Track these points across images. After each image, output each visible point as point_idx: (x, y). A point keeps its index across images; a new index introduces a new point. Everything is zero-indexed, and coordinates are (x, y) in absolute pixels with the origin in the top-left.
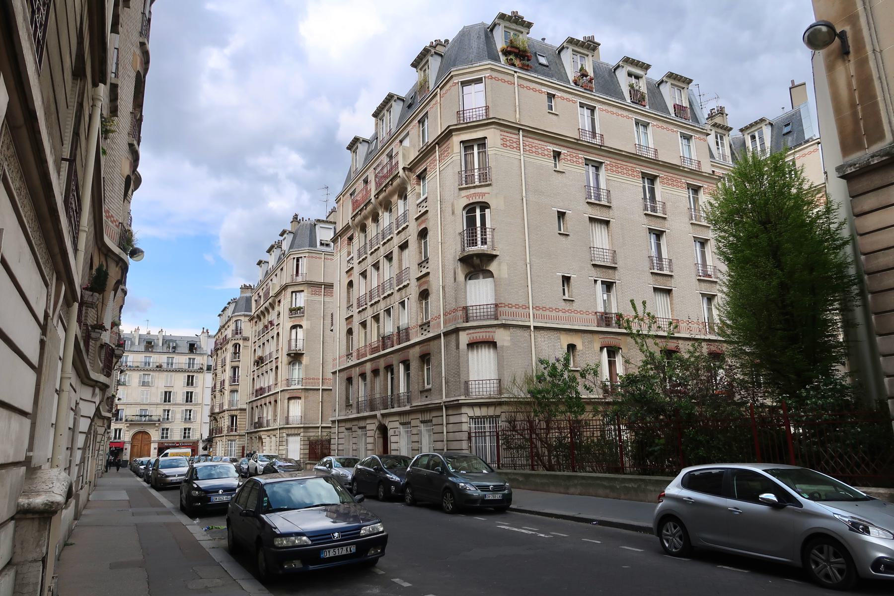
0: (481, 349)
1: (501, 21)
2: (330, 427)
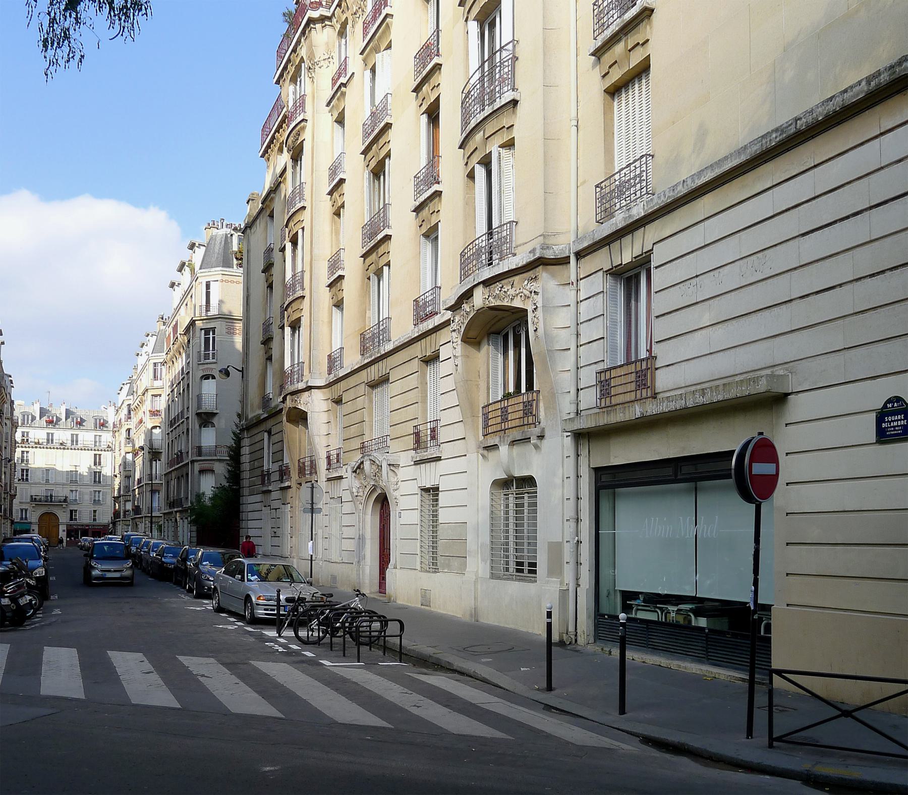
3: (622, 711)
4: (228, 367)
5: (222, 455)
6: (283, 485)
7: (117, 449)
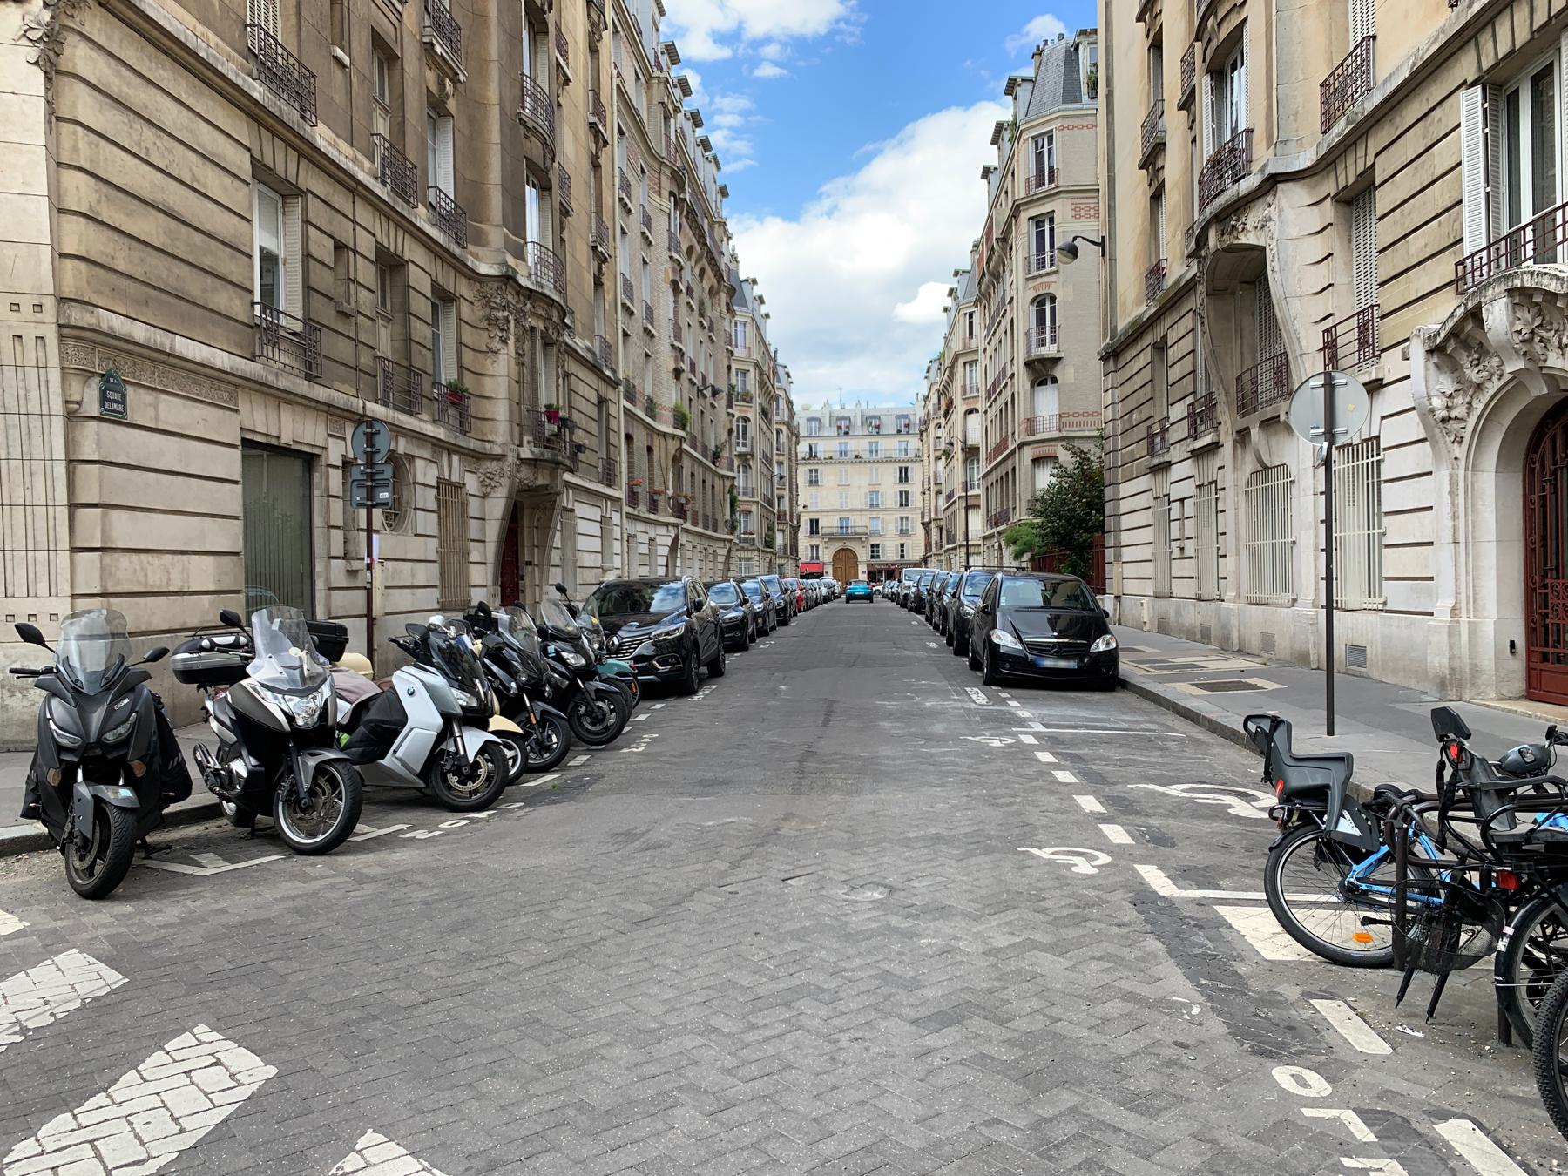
1: (1082, 38)
3: (1331, 732)
4: (1075, 239)
6: (1199, 444)
7: (925, 458)
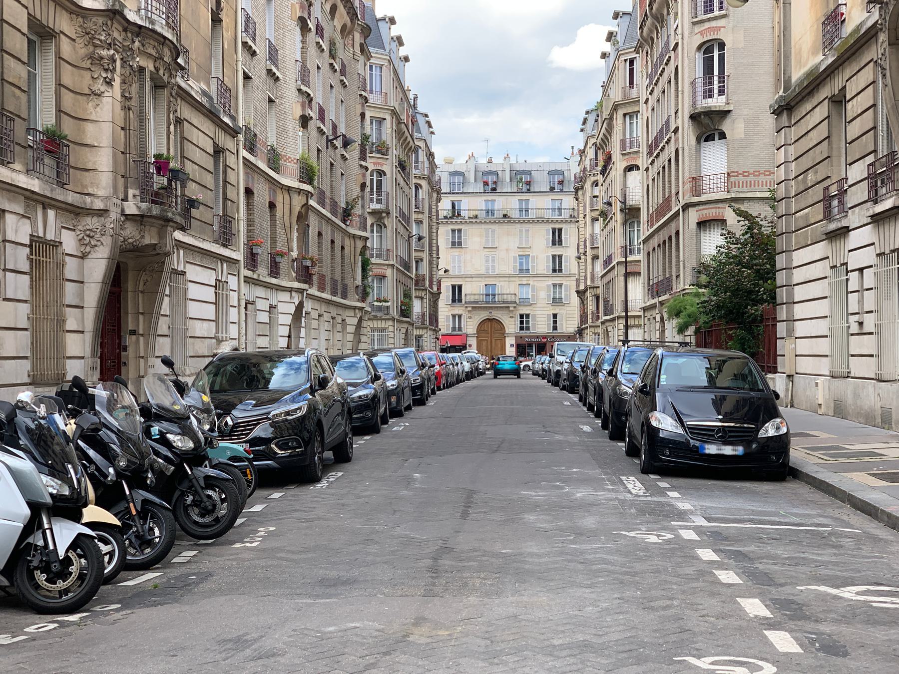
0: (710, 231)
2: (639, 317)
5: (740, 189)
